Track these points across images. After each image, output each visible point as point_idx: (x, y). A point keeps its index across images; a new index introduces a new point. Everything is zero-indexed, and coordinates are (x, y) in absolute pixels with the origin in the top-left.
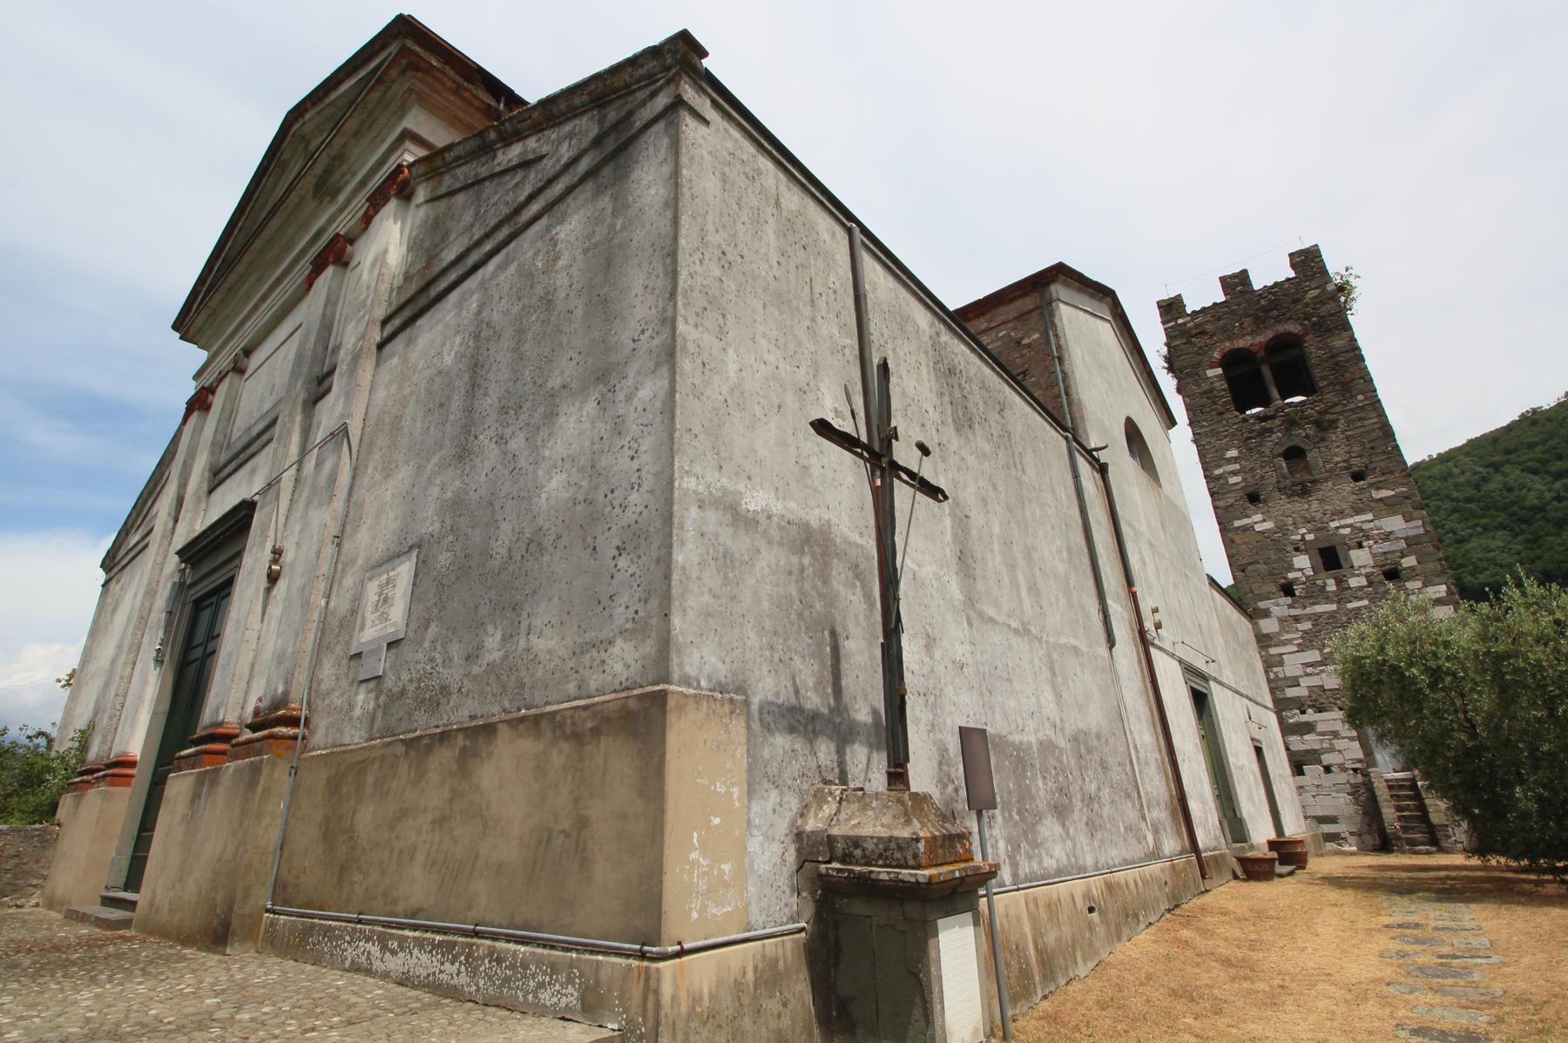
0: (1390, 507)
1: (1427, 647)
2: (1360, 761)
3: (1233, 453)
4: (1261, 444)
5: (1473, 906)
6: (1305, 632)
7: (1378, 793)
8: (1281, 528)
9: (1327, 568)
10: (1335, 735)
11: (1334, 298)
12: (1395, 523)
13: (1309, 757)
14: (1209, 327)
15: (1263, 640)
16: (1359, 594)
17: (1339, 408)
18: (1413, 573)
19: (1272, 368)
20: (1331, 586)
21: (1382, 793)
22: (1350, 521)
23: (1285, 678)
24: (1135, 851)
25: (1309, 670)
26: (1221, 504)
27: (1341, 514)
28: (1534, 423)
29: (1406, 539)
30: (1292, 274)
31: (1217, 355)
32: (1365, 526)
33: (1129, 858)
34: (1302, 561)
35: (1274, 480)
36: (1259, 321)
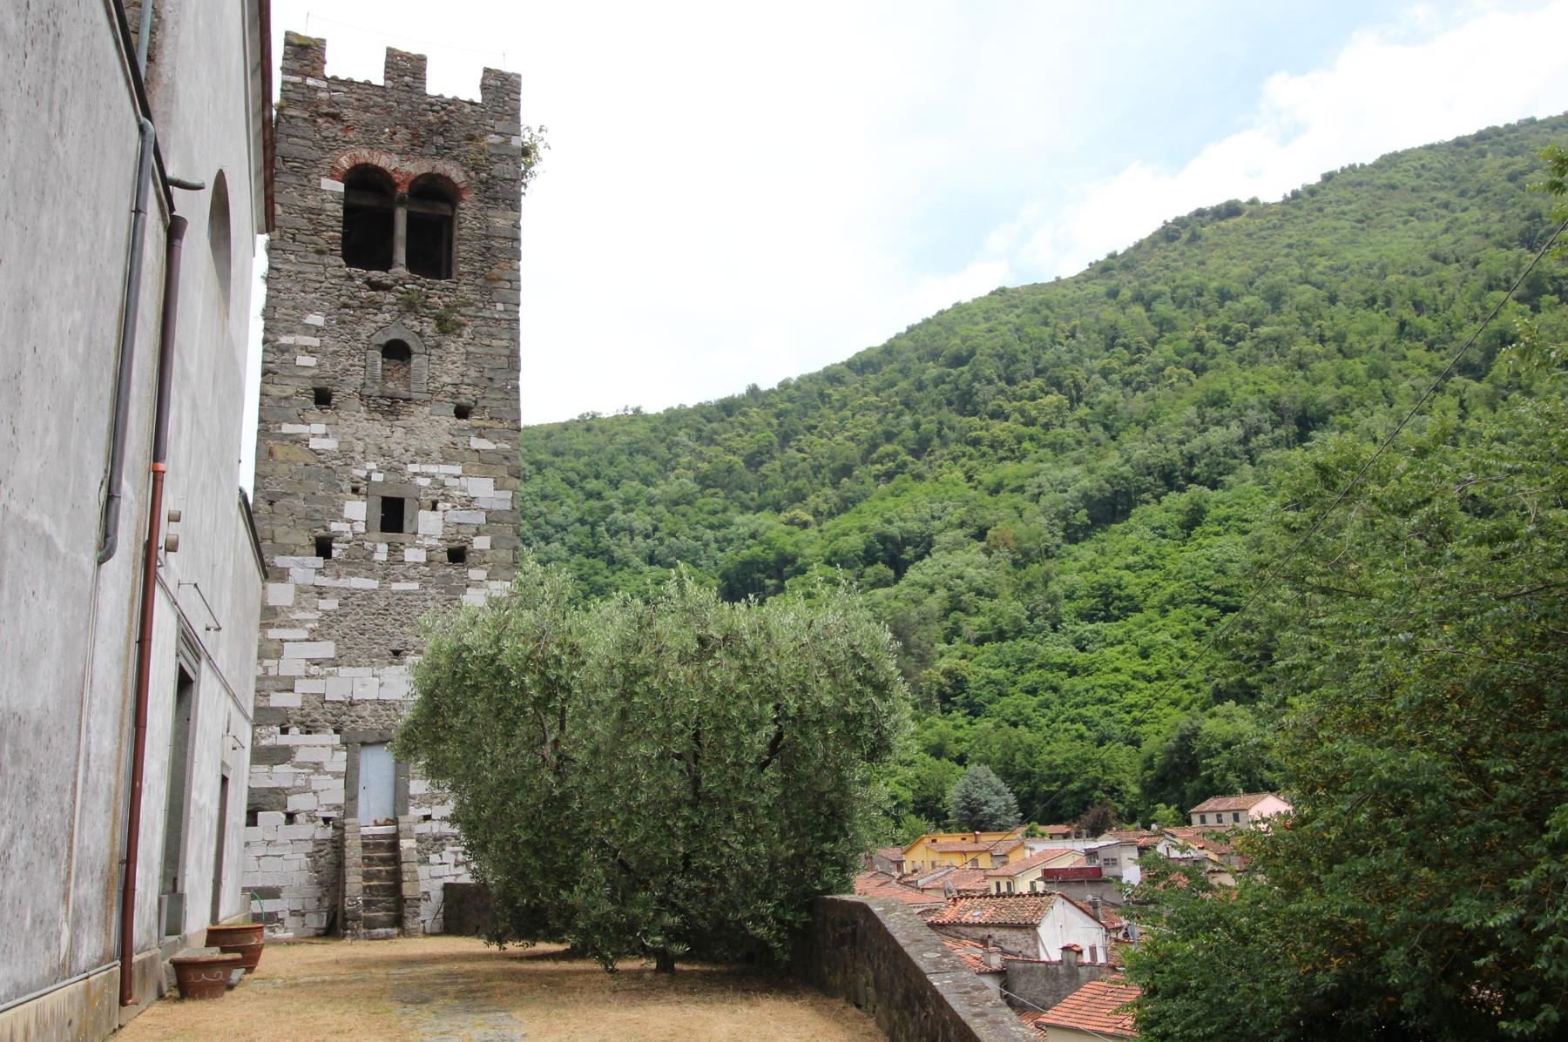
0: (484, 463)
1: (552, 647)
2: (337, 807)
3: (317, 319)
4: (358, 321)
5: (517, 1014)
7: (349, 853)
8: (345, 454)
10: (317, 767)
12: (483, 489)
13: (272, 798)
14: (349, 114)
15: (269, 615)
16: (412, 573)
17: (470, 311)
19: (412, 220)
20: (382, 554)
21: (354, 853)
22: (433, 469)
23: (277, 678)
24: (43, 963)
25: (314, 670)
26: (274, 391)
27: (425, 455)
29: (489, 512)
31: (345, 162)
32: (450, 482)
33: (23, 980)
34: (357, 510)
35: (358, 381)
36: (416, 145)
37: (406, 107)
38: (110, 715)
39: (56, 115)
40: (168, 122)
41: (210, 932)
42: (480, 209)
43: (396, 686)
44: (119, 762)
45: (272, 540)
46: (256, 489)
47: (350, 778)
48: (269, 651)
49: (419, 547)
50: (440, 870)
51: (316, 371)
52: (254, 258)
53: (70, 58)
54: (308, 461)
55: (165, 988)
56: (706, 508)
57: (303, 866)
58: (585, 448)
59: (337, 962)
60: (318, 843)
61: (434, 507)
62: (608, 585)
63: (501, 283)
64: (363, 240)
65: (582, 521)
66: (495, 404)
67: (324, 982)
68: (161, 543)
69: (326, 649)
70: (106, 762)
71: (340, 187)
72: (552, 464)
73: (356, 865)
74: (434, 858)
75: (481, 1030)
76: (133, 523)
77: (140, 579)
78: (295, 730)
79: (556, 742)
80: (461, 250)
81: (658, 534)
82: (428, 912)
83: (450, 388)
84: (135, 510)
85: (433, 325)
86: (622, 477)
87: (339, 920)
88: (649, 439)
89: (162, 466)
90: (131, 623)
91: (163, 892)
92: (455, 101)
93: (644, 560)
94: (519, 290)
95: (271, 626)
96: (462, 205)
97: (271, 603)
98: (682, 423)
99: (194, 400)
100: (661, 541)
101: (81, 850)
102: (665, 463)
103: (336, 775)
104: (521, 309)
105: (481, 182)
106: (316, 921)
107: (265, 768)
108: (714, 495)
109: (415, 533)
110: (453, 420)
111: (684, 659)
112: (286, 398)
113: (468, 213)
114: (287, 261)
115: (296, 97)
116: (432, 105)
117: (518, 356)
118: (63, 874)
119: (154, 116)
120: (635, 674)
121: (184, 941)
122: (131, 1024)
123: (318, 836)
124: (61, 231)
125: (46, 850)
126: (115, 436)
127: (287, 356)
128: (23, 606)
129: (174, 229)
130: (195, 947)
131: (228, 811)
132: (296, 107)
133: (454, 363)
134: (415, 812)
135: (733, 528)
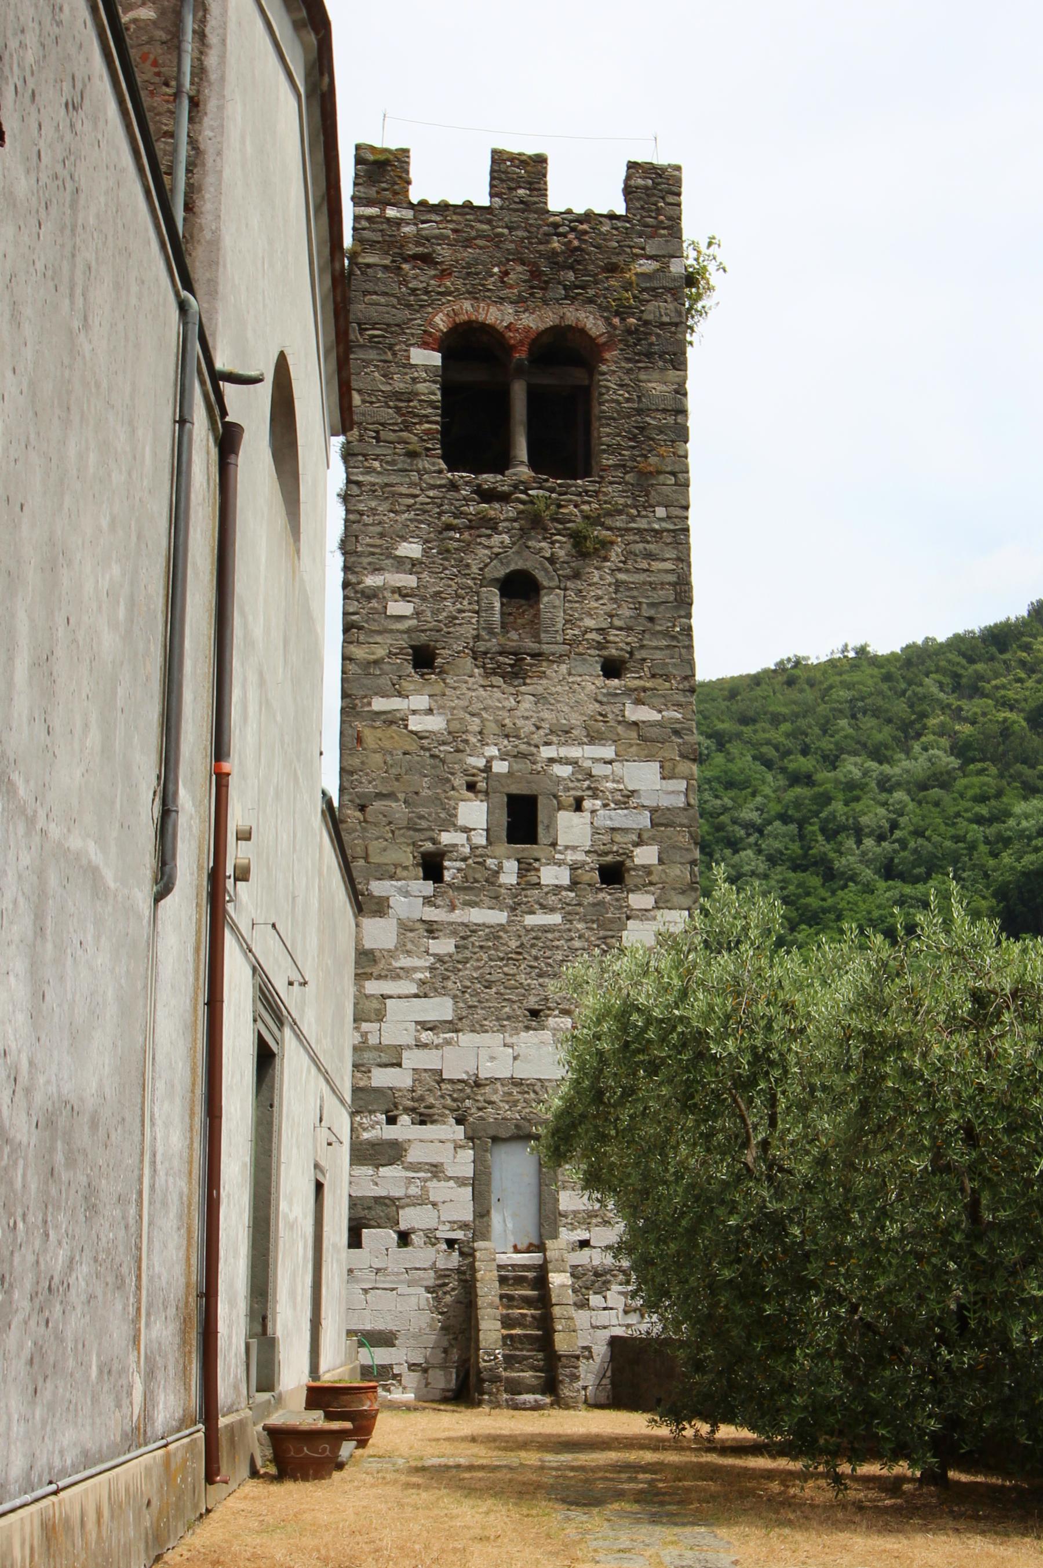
0: (645, 741)
2: (464, 1226)
3: (411, 549)
4: (467, 547)
5: (722, 1532)
6: (440, 959)
7: (482, 1289)
8: (455, 737)
9: (512, 839)
10: (436, 1170)
11: (675, 293)
12: (644, 777)
13: (379, 1211)
14: (444, 253)
15: (367, 962)
16: (552, 900)
17: (619, 522)
18: (647, 878)
19: (534, 396)
20: (509, 876)
21: (488, 1290)
22: (574, 752)
23: (379, 1048)
24: (112, 1426)
25: (426, 1036)
26: (359, 653)
27: (563, 733)
28: (791, 682)
29: (653, 811)
30: (621, 209)
31: (441, 322)
32: (598, 770)
34: (474, 813)
35: (469, 631)
36: (538, 284)
37: (520, 233)
38: (178, 1101)
39: (79, 301)
40: (213, 293)
41: (311, 1390)
42: (629, 371)
43: (540, 1059)
44: (190, 1162)
45: (366, 858)
46: (342, 790)
47: (480, 1184)
48: (368, 1012)
49: (559, 864)
50: (600, 1321)
51: (414, 622)
52: (325, 469)
53: (92, 221)
54: (407, 748)
55: (259, 1462)
56: (970, 793)
57: (423, 1304)
58: (784, 710)
59: (473, 1439)
60: (442, 1275)
61: (578, 807)
62: (825, 911)
63: (661, 477)
64: (470, 432)
65: (785, 818)
66: (658, 655)
67: (458, 1466)
68: (229, 871)
69: (441, 1008)
70: (176, 1163)
71: (435, 359)
72: (739, 735)
73: (491, 1305)
74: (595, 1300)
75: (674, 1551)
76: (194, 845)
77: (206, 920)
78: (405, 1119)
79: (765, 1145)
80: (605, 434)
81: (898, 834)
82: (588, 1375)
83: (593, 636)
84: (195, 823)
85: (569, 546)
86: (842, 750)
87: (473, 1379)
88: (880, 693)
89: (226, 767)
90: (197, 979)
91: (251, 1335)
92: (589, 217)
93: (877, 872)
94: (686, 485)
95: (369, 976)
96: (604, 368)
97: (368, 945)
98: (930, 664)
99: (261, 674)
100: (903, 844)
101: (151, 1279)
102: (905, 727)
103: (461, 1182)
104: (691, 513)
105: (629, 332)
106: (442, 1381)
107: (368, 1170)
108: (980, 772)
109: (554, 844)
110: (600, 681)
111: (954, 1024)
112: (376, 662)
113: (612, 377)
114: (370, 470)
115: (377, 237)
116: (556, 226)
117: (689, 584)
118: (131, 1310)
119: (196, 286)
120: (877, 1047)
121: (279, 1400)
122: (220, 1508)
123: (441, 1265)
124: (92, 458)
125: (110, 1279)
126: (168, 729)
127: (374, 603)
128: (69, 961)
129: (228, 440)
130: (293, 1412)
131: (326, 1228)
132: (375, 244)
133: (598, 598)
134: (568, 1236)
135: (1011, 822)
